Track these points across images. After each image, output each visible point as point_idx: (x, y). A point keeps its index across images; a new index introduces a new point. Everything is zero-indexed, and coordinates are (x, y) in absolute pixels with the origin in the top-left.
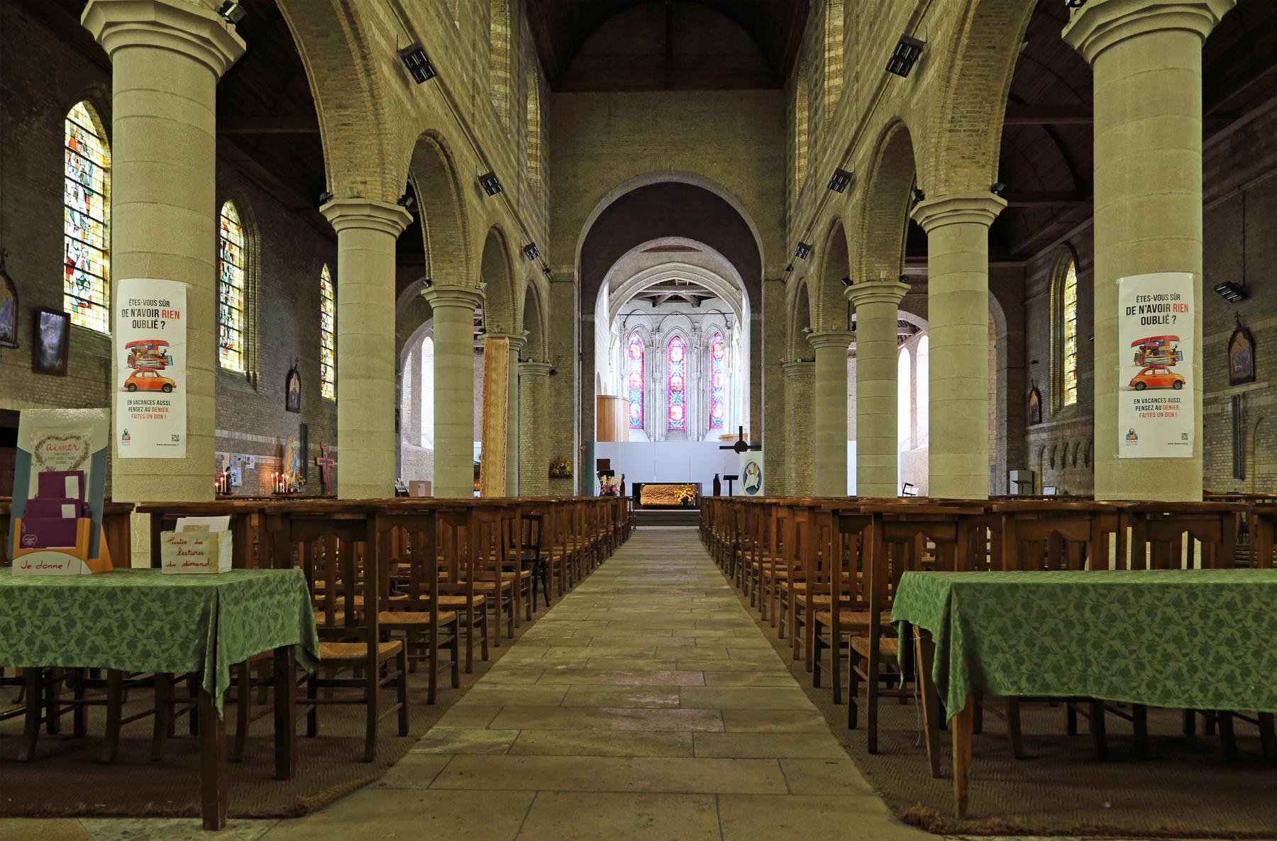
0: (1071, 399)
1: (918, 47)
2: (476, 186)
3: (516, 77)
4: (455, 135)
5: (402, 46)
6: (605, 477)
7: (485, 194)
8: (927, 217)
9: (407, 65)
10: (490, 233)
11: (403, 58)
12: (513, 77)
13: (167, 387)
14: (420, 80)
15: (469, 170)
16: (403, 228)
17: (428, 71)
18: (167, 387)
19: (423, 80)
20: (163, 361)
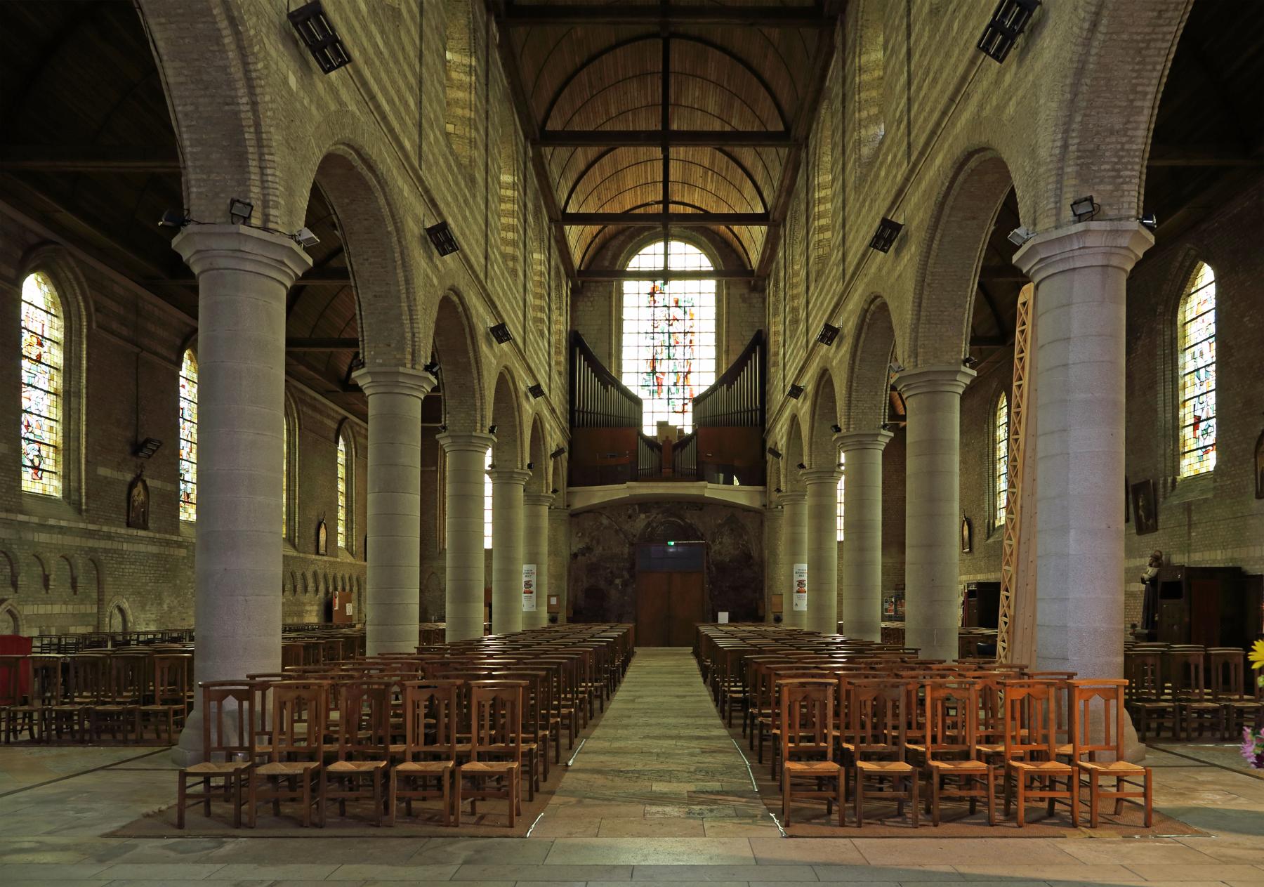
0: (247, 688)
1: (897, 227)
2: (423, 238)
3: (484, 102)
4: (395, 172)
5: (428, 226)
6: (286, 783)
7: (436, 252)
8: (1041, 260)
9: (432, 240)
10: (501, 373)
11: (295, 25)
12: (479, 117)
13: (531, 593)
14: (500, 342)
15: (484, 320)
16: (296, 275)
17: (338, 54)
18: (531, 593)
19: (332, 68)
20: (531, 586)
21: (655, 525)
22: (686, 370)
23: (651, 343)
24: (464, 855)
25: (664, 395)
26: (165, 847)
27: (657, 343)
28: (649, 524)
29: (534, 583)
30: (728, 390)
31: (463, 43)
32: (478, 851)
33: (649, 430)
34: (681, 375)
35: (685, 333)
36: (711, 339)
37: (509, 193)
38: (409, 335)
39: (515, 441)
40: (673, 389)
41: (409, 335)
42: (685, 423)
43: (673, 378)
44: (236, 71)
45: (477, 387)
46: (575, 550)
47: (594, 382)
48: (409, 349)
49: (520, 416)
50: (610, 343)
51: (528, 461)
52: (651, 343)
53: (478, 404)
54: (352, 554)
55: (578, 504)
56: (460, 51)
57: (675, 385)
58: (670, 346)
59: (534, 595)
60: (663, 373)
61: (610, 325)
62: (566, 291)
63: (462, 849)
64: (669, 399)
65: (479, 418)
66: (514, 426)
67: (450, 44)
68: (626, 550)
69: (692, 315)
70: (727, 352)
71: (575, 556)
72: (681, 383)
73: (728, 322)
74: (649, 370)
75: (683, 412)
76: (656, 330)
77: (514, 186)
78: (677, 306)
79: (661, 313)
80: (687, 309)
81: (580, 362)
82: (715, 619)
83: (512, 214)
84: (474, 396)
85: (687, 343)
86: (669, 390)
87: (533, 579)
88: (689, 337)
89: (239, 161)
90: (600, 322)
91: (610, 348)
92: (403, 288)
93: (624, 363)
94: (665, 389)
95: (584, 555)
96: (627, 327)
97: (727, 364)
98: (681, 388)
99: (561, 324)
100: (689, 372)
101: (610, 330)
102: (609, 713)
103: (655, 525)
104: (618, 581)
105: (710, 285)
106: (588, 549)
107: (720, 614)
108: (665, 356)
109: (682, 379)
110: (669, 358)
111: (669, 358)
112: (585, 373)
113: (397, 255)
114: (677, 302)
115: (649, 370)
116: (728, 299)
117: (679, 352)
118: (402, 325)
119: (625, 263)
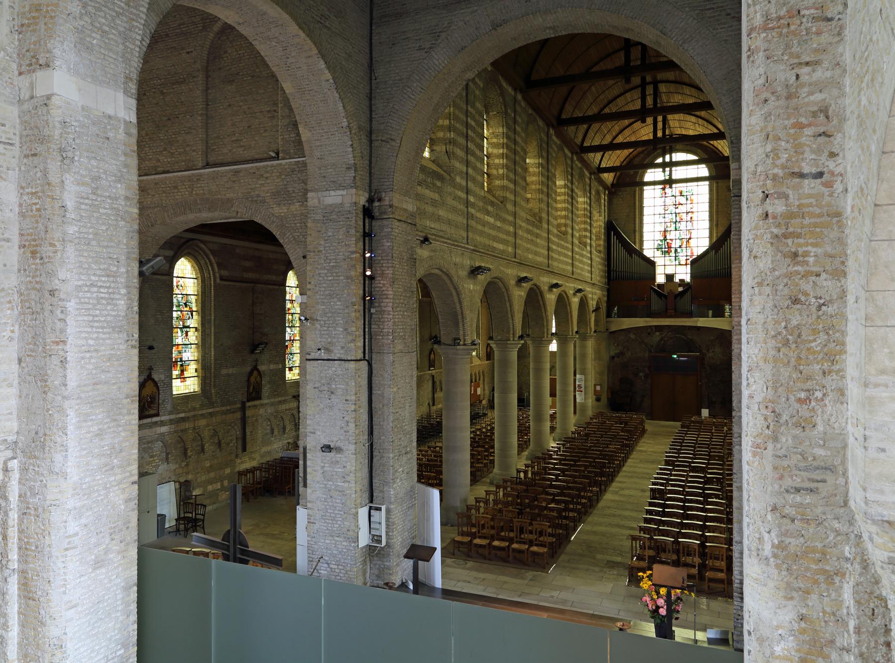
21: (666, 339)
22: (688, 237)
23: (663, 220)
24: (530, 577)
25: (673, 254)
26: (453, 562)
27: (667, 220)
28: (662, 339)
29: (583, 386)
30: (715, 254)
31: (536, 153)
32: (534, 576)
33: (660, 279)
34: (685, 241)
35: (687, 213)
36: (706, 216)
37: (563, 190)
38: (511, 326)
39: (568, 321)
40: (679, 250)
41: (511, 326)
42: (684, 274)
43: (678, 243)
44: (456, 300)
45: (544, 316)
46: (612, 353)
47: (623, 253)
48: (512, 332)
49: (570, 308)
50: (635, 224)
51: (576, 329)
52: (663, 220)
53: (545, 324)
54: (479, 358)
55: (613, 328)
56: (534, 157)
57: (680, 247)
58: (676, 221)
59: (583, 393)
60: (672, 240)
61: (635, 212)
62: (604, 198)
63: (530, 574)
64: (676, 256)
65: (545, 330)
66: (567, 313)
67: (529, 155)
68: (647, 355)
69: (691, 200)
70: (717, 225)
71: (613, 358)
72: (684, 245)
73: (717, 206)
74: (662, 238)
75: (686, 264)
76: (666, 212)
77: (565, 186)
78: (681, 195)
79: (670, 201)
80: (688, 197)
81: (613, 238)
82: (699, 414)
83: (564, 201)
84: (543, 320)
85: (689, 219)
86: (676, 251)
87: (583, 384)
88: (690, 215)
89: (456, 324)
90: (627, 210)
91: (635, 227)
92: (509, 309)
93: (645, 235)
94: (673, 250)
95: (619, 357)
96: (646, 211)
97: (717, 233)
98: (684, 249)
99: (600, 221)
100: (690, 238)
101: (635, 215)
102: (602, 504)
103: (666, 339)
104: (641, 374)
105: (704, 187)
106: (622, 354)
107: (703, 410)
108: (673, 228)
109: (685, 243)
110: (676, 230)
111: (676, 230)
112: (618, 251)
113: (506, 298)
114: (681, 193)
115: (662, 238)
116: (717, 190)
117: (682, 226)
118: (509, 323)
119: (643, 176)
